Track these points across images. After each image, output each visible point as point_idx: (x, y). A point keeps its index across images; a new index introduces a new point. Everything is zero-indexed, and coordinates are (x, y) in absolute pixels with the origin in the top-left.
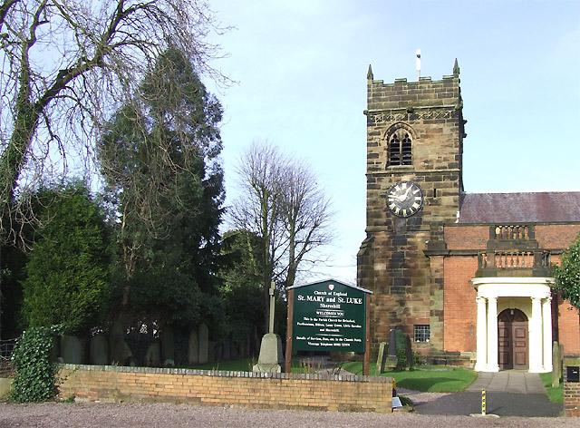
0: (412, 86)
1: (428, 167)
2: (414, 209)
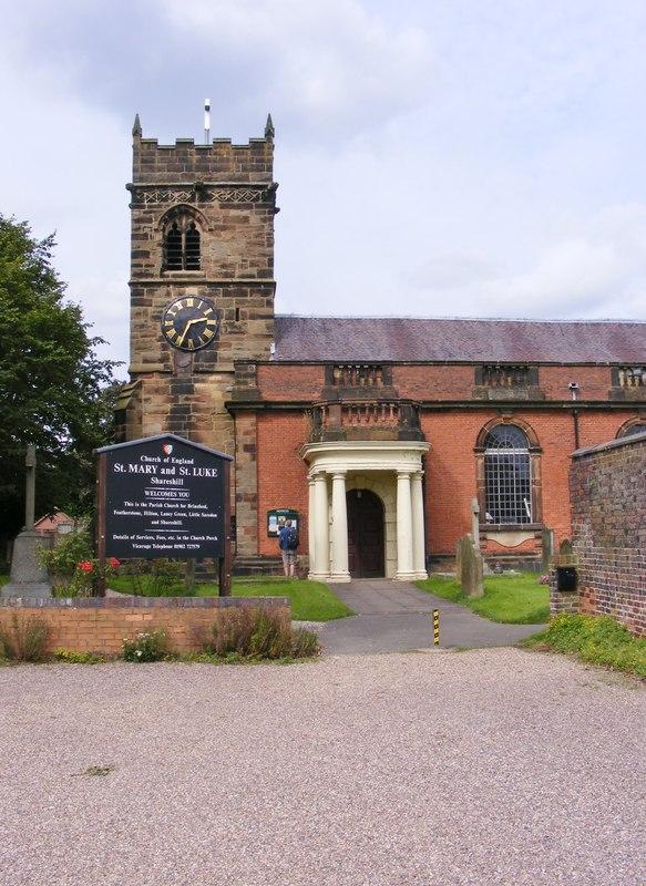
0: (203, 150)
1: (226, 275)
2: (206, 339)
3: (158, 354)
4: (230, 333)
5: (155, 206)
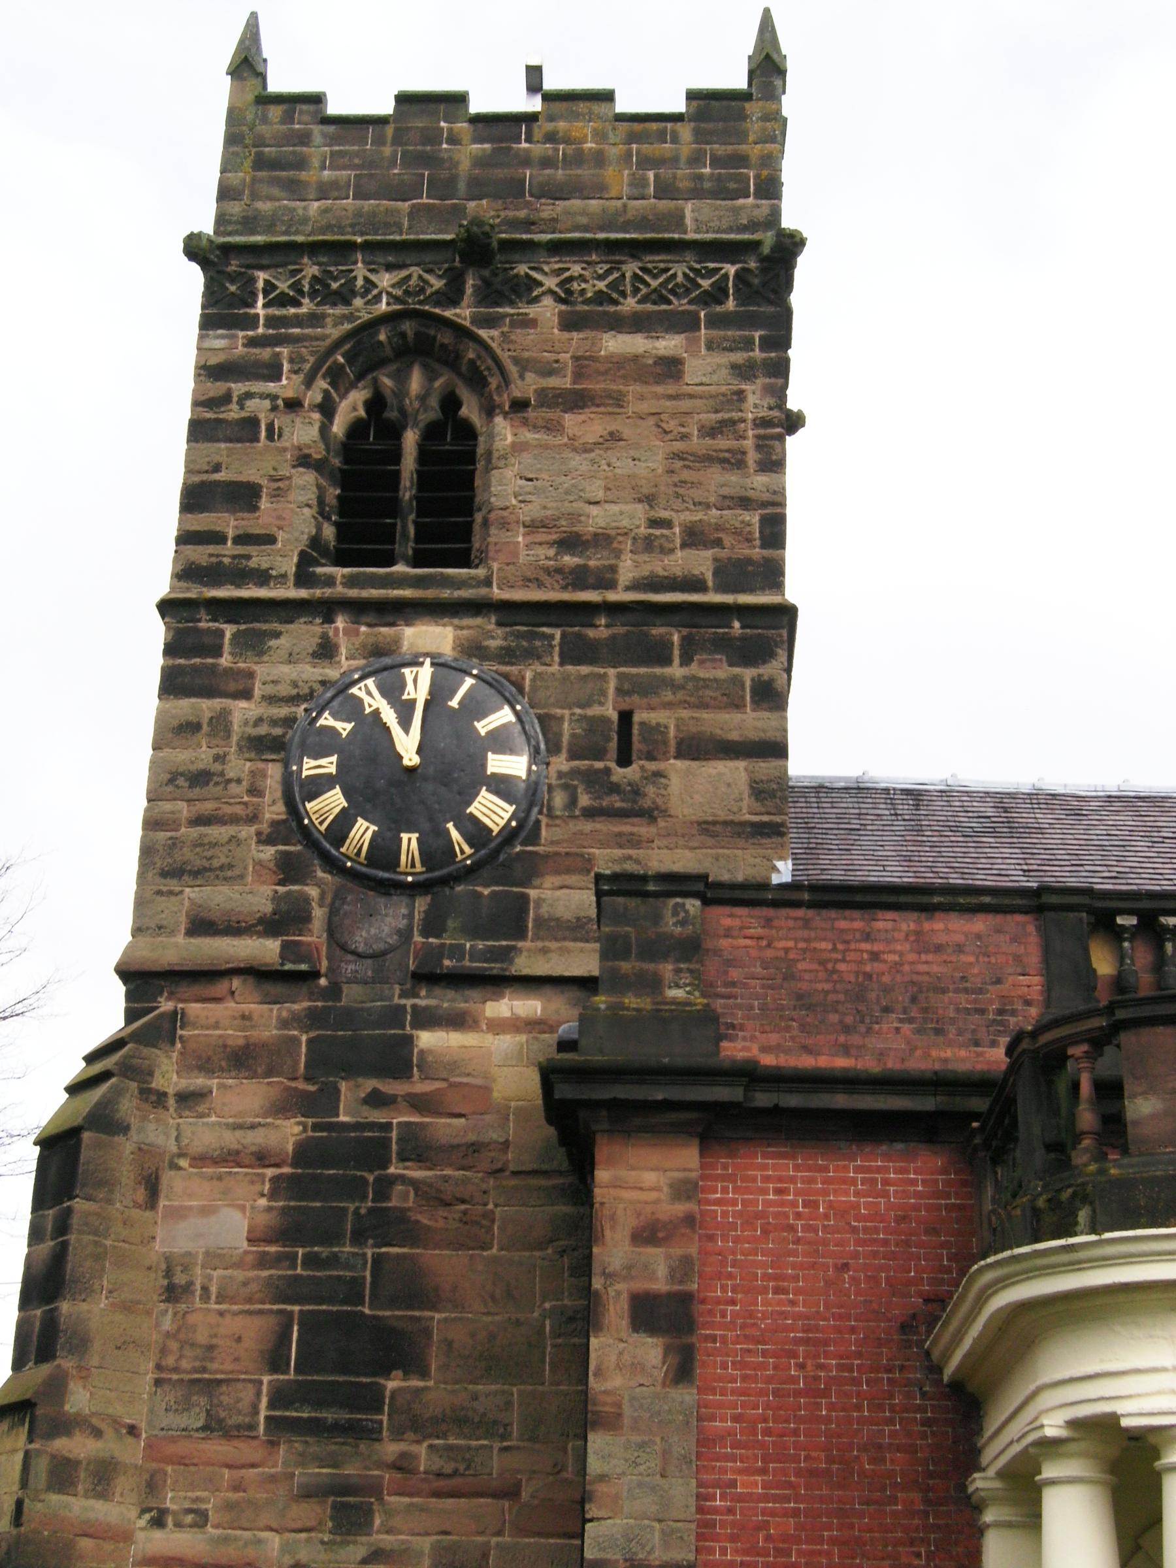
1: (579, 578)
2: (476, 832)
3: (258, 896)
4: (590, 813)
5: (298, 321)
